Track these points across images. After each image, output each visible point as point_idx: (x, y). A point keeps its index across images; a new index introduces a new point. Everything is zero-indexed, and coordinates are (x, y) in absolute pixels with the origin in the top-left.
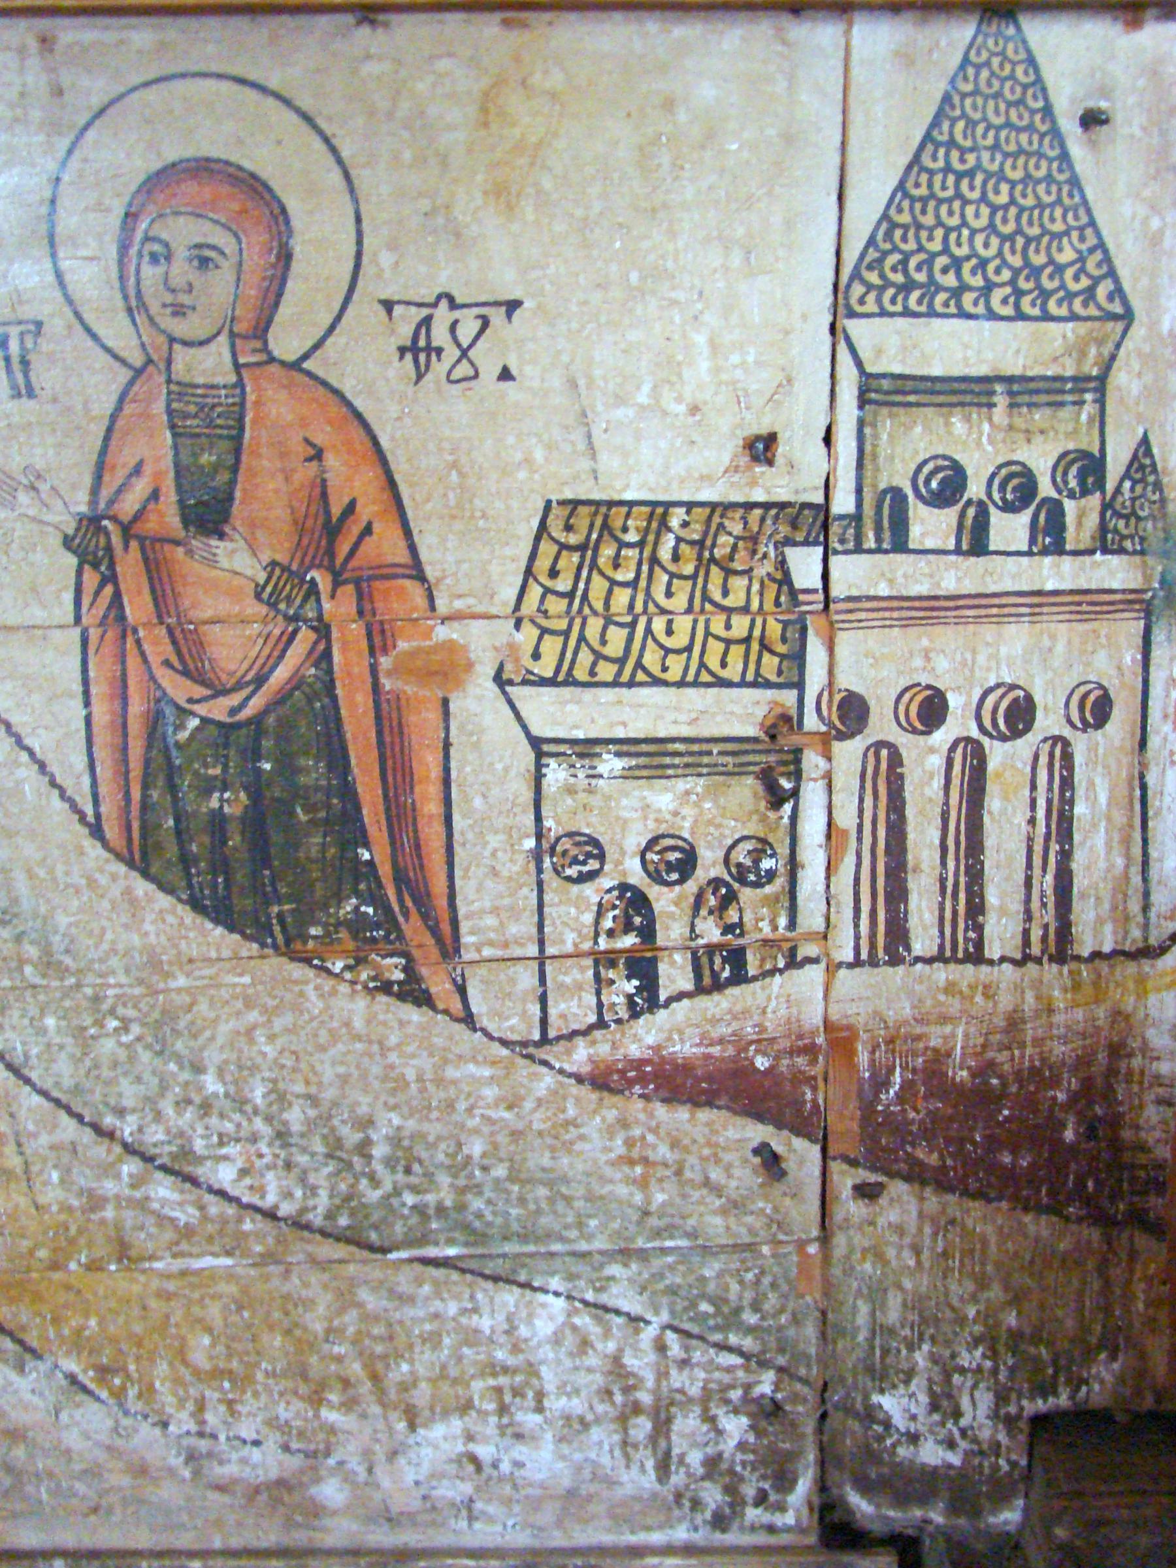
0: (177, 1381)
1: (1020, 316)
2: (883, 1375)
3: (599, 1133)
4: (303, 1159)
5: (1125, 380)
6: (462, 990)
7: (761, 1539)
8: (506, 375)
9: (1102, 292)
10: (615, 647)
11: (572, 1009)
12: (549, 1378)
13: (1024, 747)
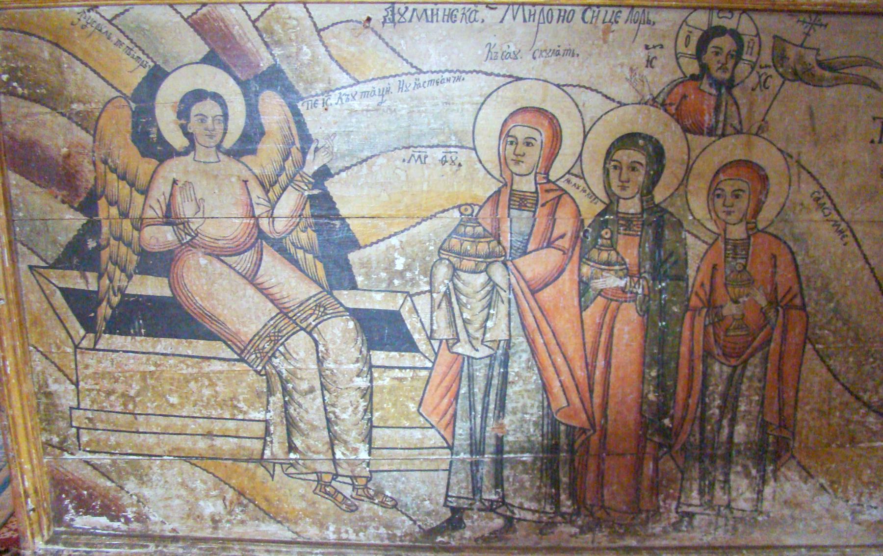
0: (855, 486)
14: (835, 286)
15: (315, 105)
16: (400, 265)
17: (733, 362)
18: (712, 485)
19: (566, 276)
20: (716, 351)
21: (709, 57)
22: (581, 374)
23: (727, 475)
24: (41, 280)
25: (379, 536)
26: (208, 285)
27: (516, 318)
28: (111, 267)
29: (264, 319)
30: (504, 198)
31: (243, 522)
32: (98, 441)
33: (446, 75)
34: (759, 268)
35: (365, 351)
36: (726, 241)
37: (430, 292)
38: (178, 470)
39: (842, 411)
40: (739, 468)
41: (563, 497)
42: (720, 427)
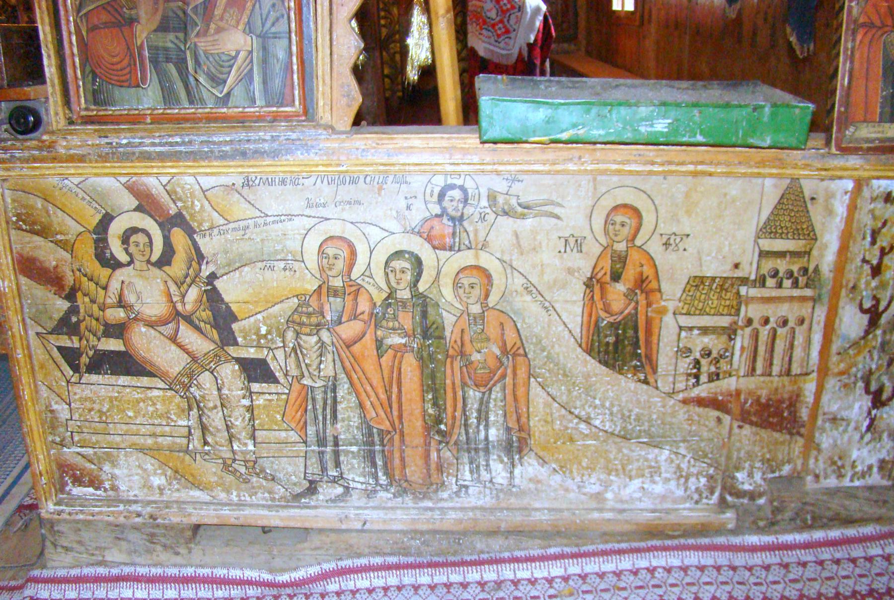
0: (578, 469)
1: (794, 239)
2: (737, 468)
3: (682, 413)
4: (615, 419)
5: (815, 253)
6: (656, 381)
7: (706, 506)
8: (685, 250)
9: (811, 234)
10: (700, 306)
11: (681, 386)
12: (663, 469)
13: (785, 330)
14: (545, 342)
15: (204, 236)
16: (263, 330)
17: (482, 389)
18: (478, 467)
19: (367, 335)
20: (470, 382)
21: (446, 204)
22: (383, 396)
23: (487, 461)
24: (45, 342)
25: (264, 499)
26: (148, 343)
27: (338, 364)
28: (87, 333)
29: (183, 364)
30: (324, 290)
31: (178, 490)
32: (85, 440)
33: (283, 218)
34: (492, 331)
35: (246, 383)
36: (469, 315)
37: (284, 347)
38: (134, 458)
39: (561, 421)
40: (495, 457)
41: (380, 474)
42: (478, 432)
